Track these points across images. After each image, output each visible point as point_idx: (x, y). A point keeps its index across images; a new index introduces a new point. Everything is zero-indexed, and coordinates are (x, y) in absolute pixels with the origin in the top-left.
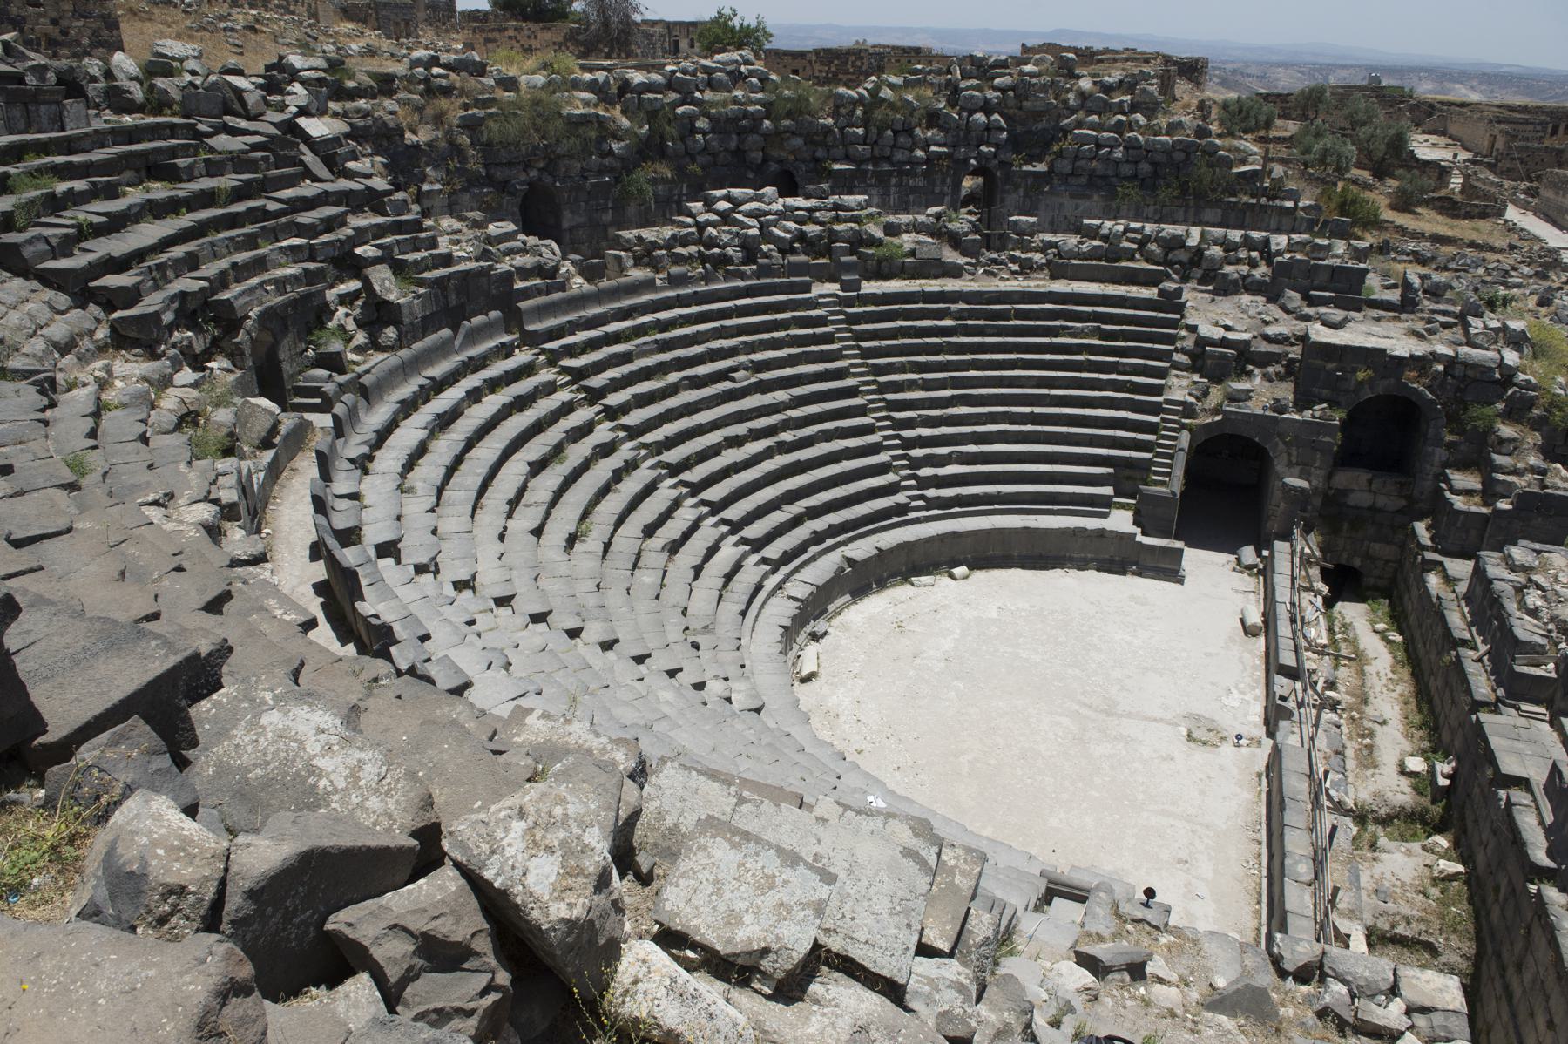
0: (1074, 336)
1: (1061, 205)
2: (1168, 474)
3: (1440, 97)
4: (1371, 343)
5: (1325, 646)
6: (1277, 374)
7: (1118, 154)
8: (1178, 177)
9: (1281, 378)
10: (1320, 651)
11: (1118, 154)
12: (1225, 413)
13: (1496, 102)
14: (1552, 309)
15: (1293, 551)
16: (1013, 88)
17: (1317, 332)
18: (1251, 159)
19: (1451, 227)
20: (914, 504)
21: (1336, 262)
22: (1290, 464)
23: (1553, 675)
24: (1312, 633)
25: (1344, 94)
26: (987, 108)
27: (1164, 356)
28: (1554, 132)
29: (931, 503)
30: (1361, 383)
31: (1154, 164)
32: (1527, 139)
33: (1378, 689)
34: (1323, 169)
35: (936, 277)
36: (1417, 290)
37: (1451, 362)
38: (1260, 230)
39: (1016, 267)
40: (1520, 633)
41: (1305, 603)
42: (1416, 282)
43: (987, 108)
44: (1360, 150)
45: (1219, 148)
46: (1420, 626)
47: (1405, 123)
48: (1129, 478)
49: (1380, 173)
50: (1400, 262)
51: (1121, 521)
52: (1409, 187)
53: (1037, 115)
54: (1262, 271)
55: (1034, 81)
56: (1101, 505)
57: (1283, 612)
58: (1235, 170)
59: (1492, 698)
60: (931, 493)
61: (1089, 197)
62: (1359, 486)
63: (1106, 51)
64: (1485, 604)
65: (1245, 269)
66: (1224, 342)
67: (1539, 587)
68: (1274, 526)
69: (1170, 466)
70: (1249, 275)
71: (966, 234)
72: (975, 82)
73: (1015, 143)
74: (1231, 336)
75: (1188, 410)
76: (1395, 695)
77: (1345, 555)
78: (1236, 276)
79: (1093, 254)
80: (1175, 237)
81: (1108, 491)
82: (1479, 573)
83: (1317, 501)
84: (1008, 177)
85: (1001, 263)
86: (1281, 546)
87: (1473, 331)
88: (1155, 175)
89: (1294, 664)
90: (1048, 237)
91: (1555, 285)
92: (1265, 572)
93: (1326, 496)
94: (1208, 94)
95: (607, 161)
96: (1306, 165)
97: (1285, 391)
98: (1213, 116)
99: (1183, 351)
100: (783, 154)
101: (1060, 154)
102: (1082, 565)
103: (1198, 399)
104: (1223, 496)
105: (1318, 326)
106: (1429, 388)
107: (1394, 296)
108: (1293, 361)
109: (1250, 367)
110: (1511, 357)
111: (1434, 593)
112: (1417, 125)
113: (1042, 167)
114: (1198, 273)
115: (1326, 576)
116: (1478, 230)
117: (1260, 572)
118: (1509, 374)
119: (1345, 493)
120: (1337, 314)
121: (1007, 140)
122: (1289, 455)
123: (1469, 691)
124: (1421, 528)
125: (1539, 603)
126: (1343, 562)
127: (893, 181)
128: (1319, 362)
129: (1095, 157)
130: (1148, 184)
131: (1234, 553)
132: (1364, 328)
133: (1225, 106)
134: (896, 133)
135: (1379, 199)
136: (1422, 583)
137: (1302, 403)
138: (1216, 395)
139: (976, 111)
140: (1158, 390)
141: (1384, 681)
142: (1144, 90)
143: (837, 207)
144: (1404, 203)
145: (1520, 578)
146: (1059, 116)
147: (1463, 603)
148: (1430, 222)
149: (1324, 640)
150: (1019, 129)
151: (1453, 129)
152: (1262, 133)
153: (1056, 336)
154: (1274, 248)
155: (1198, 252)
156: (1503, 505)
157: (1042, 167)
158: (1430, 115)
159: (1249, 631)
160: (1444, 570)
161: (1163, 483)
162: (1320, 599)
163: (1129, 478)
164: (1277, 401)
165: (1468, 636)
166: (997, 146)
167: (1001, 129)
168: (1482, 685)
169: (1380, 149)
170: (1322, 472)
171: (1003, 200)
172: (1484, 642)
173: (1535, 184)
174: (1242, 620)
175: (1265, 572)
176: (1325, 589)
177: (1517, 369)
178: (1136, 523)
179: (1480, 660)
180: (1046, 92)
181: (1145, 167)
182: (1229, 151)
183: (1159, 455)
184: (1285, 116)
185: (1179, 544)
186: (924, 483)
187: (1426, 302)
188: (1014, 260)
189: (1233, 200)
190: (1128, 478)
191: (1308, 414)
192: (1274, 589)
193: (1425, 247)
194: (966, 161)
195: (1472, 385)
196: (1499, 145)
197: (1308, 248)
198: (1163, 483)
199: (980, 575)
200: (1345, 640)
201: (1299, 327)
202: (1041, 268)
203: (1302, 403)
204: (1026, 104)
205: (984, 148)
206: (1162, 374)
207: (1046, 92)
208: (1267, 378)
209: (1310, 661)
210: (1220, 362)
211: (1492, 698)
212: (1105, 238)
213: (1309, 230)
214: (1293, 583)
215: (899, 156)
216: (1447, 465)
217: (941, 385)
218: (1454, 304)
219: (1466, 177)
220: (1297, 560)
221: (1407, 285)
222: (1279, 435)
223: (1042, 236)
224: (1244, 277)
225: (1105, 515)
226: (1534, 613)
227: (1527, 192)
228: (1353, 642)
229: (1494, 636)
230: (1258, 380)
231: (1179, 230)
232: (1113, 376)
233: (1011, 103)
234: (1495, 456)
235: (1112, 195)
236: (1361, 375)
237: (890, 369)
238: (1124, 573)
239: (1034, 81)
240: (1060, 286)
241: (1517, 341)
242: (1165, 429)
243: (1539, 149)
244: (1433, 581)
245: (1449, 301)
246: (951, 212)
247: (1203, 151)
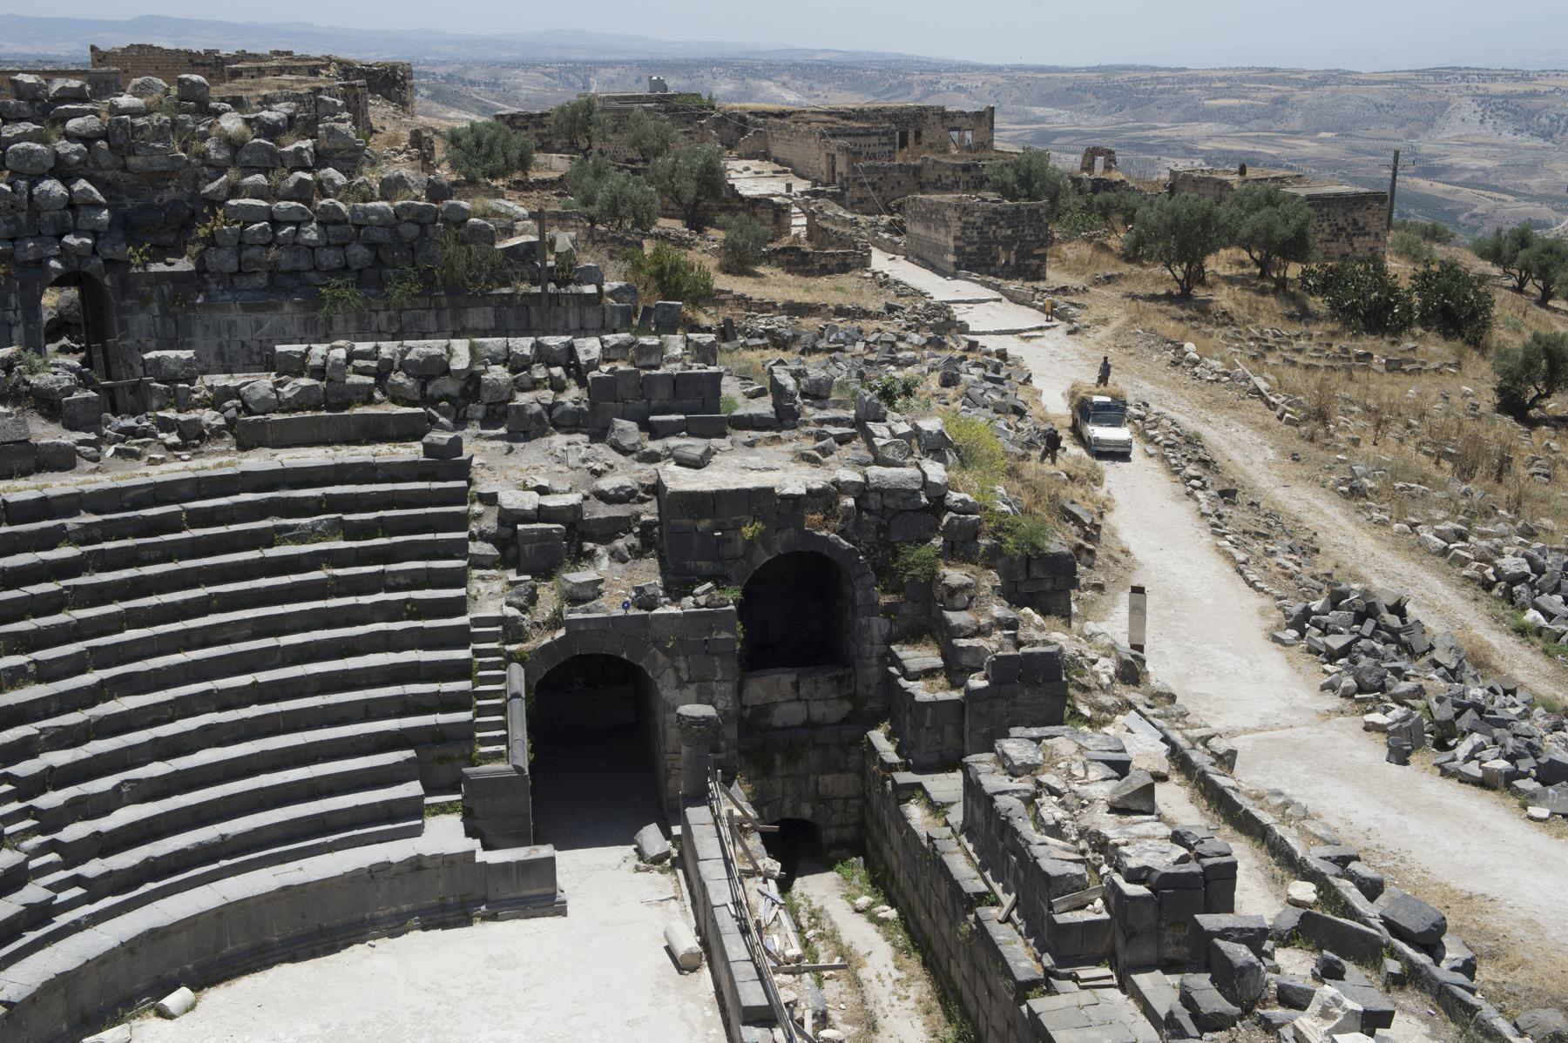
0: (301, 539)
1: (232, 324)
2: (503, 740)
3: (752, 106)
4: (751, 481)
5: (799, 959)
6: (630, 548)
7: (311, 233)
8: (410, 264)
9: (638, 554)
10: (794, 968)
11: (311, 233)
12: (569, 624)
13: (825, 108)
14: (961, 388)
15: (717, 819)
16: (104, 136)
17: (674, 478)
18: (519, 226)
19: (808, 290)
20: (63, 897)
21: (674, 368)
22: (681, 684)
23: (1105, 916)
24: (775, 942)
25: (621, 112)
26: (63, 171)
27: (449, 550)
28: (904, 143)
29: (95, 888)
30: (750, 543)
31: (373, 246)
32: (873, 156)
33: (885, 1003)
34: (616, 223)
35: (25, 474)
36: (792, 395)
37: (862, 491)
38: (555, 332)
39: (173, 438)
40: (1051, 867)
41: (754, 897)
42: (790, 383)
43: (63, 171)
44: (663, 191)
45: (468, 214)
46: (916, 887)
47: (712, 146)
48: (441, 759)
49: (697, 222)
50: (752, 348)
51: (444, 835)
52: (741, 241)
53: (158, 179)
54: (573, 395)
55: (140, 121)
56: (406, 816)
57: (726, 921)
58: (500, 246)
59: (1040, 973)
60: (93, 868)
61: (277, 307)
62: (784, 695)
63: (242, 56)
64: (990, 830)
65: (547, 395)
66: (542, 514)
67: (1053, 791)
68: (679, 785)
69: (502, 725)
70: (555, 405)
71: (69, 391)
72: (30, 127)
73: (128, 226)
74: (551, 501)
75: (511, 630)
76: (910, 1004)
77: (788, 804)
78: (537, 407)
79: (303, 401)
80: (431, 359)
81: (413, 788)
82: (972, 788)
83: (732, 732)
84: (126, 285)
85: (145, 433)
86: (697, 815)
87: (879, 442)
88: (378, 262)
89: (764, 1002)
90: (220, 380)
91: (957, 354)
92: (683, 860)
93: (741, 719)
94: (421, 119)
96: (592, 220)
97: (648, 574)
98: (439, 154)
99: (483, 537)
101: (211, 241)
102: (395, 927)
103: (523, 609)
104: (592, 757)
105: (672, 467)
106: (842, 533)
107: (763, 407)
108: (647, 526)
109: (589, 546)
110: (936, 472)
111: (922, 832)
112: (730, 147)
113: (184, 265)
114: (478, 410)
115: (773, 845)
116: (842, 290)
117: (675, 863)
118: (938, 495)
119: (765, 709)
120: (694, 446)
121: (111, 223)
122: (677, 670)
123: (1007, 971)
124: (878, 737)
125: (1060, 814)
126: (788, 815)
128: (686, 522)
129: (274, 242)
130: (371, 277)
131: (630, 841)
132: (735, 460)
133: (454, 138)
135: (703, 256)
136: (903, 819)
137: (677, 586)
138: (548, 599)
140: (458, 607)
141: (890, 986)
142: (331, 131)
144: (739, 262)
145: (1025, 784)
146: (197, 177)
147: (963, 838)
148: (777, 285)
149: (795, 950)
150: (129, 203)
151: (777, 149)
152: (517, 176)
153: (270, 545)
154: (583, 358)
155: (472, 380)
156: (977, 682)
157: (184, 265)
158: (743, 132)
159: (684, 966)
160: (926, 794)
161: (498, 756)
162: (772, 883)
163: (441, 759)
164: (640, 590)
165: (983, 888)
166: (95, 234)
167: (98, 206)
168: (1023, 959)
169: (689, 190)
170: (727, 687)
171: (124, 325)
172: (1006, 890)
173: (897, 217)
174: (669, 949)
175: (683, 860)
176: (776, 867)
177: (946, 487)
178: (470, 832)
179: (1008, 919)
180: (166, 140)
181: (359, 253)
182: (484, 216)
183: (482, 711)
184: (546, 148)
185: (545, 851)
186: (75, 854)
187: (809, 410)
188: (166, 425)
189: (506, 290)
190: (441, 760)
191: (688, 601)
192: (703, 887)
193: (780, 322)
194: (41, 263)
195: (897, 518)
196: (841, 166)
197: (632, 353)
198: (498, 756)
199: (216, 996)
200: (821, 937)
201: (647, 472)
202: (218, 433)
203: (677, 586)
205: (70, 239)
206: (457, 579)
207: (166, 140)
208: (617, 557)
209: (787, 989)
210: (543, 545)
211: (1040, 973)
212: (319, 372)
213: (626, 326)
214: (729, 869)
216: (891, 639)
217: (77, 665)
218: (846, 408)
219: (811, 216)
220: (725, 831)
221: (778, 390)
222: (655, 643)
223: (208, 380)
224: (550, 408)
225: (416, 832)
226: (1056, 830)
227: (890, 228)
228: (832, 937)
229: (1016, 878)
230: (605, 563)
231: (435, 346)
232: (381, 597)
233: (106, 160)
234: (949, 615)
235: (314, 300)
236: (748, 531)
238: (467, 921)
239: (140, 121)
240: (259, 461)
241: (936, 447)
242: (483, 666)
243: (891, 168)
244: (916, 813)
245: (838, 404)
246: (30, 355)
247: (446, 220)
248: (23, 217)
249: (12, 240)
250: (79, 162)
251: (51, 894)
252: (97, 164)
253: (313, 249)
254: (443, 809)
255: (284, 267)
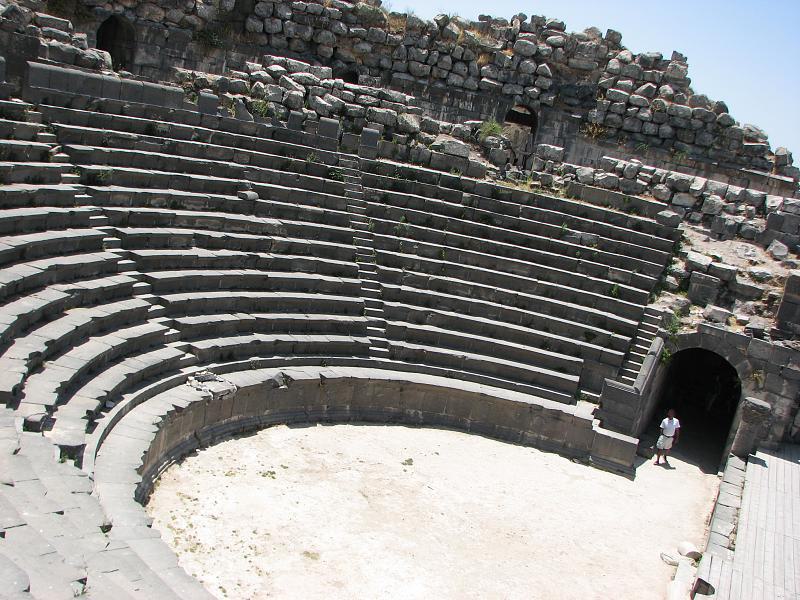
7: (646, 114)
20: (154, 308)
26: (538, 58)
31: (675, 128)
66: (709, 269)
88: (675, 137)
95: (191, 18)
100: (352, 56)
108: (773, 298)
114: (698, 216)
127: (445, 100)
134: (455, 61)
139: (527, 58)
143: (381, 96)
150: (564, 82)
155: (701, 198)
181: (667, 129)
204: (572, 61)
215: (454, 79)
237: (388, 229)
248: (512, 73)
249: (504, 83)
250: (547, 56)
251: (148, 304)
252: (555, 58)
253: (643, 122)
254: (589, 400)
255: (625, 128)
